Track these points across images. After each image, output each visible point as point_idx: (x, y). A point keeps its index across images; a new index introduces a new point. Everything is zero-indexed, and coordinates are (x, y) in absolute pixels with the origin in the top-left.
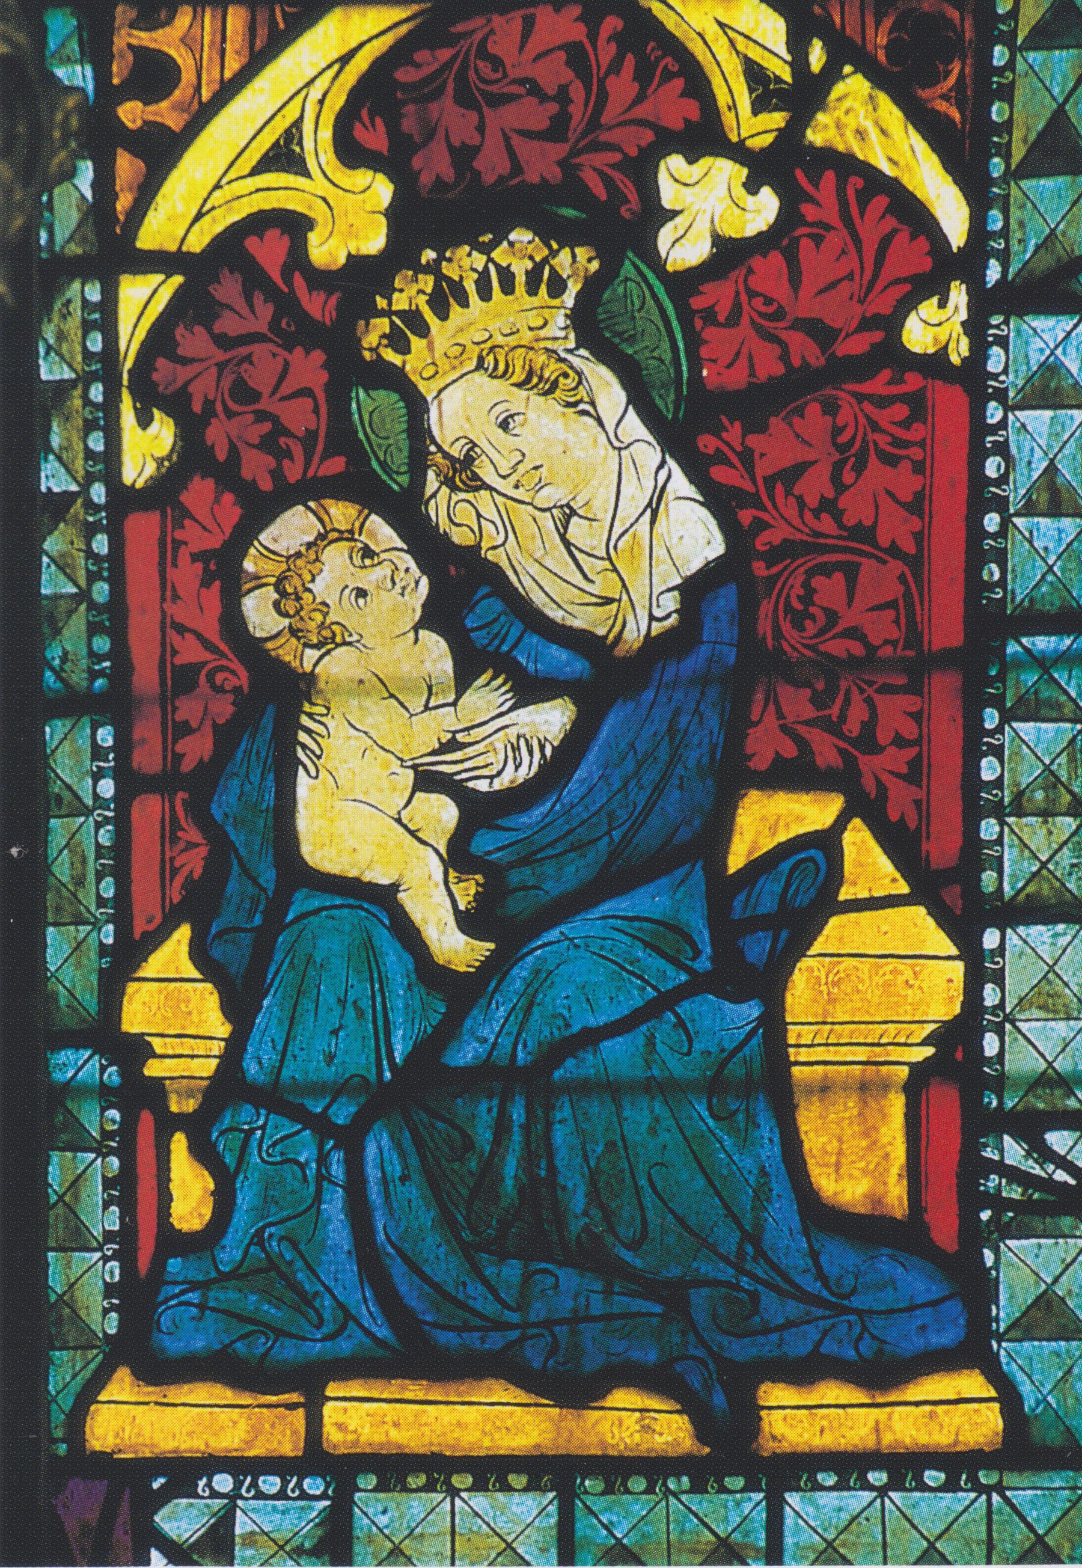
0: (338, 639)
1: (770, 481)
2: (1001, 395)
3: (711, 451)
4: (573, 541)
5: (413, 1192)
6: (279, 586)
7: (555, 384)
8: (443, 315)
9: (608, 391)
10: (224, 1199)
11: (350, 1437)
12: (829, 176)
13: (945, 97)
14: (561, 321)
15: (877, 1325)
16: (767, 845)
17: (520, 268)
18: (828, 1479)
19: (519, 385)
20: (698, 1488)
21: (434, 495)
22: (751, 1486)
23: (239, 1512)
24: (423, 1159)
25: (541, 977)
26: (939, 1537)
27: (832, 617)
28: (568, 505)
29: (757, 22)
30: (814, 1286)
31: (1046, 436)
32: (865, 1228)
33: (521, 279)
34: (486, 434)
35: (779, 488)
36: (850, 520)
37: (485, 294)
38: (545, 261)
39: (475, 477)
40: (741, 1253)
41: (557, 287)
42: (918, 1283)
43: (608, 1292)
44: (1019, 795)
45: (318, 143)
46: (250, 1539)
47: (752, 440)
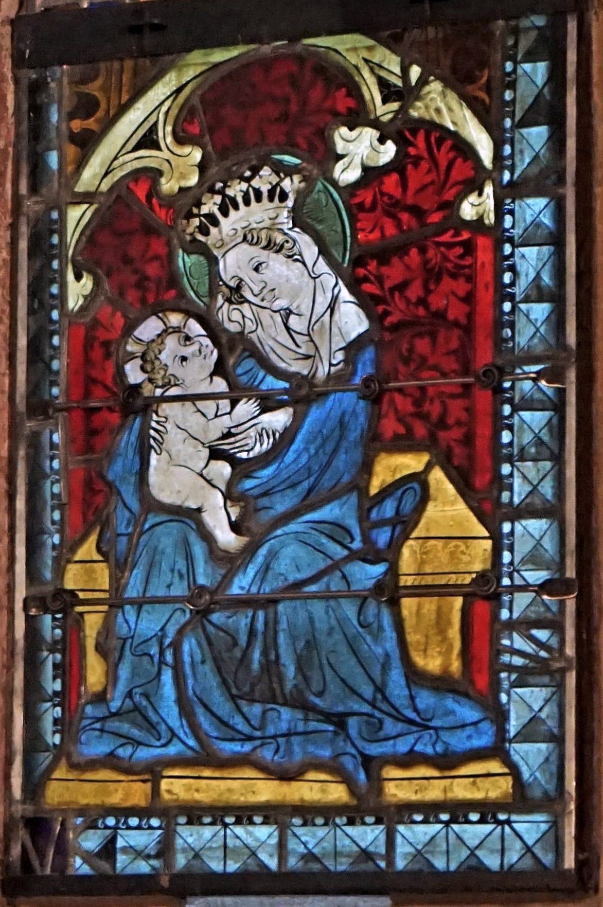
0: (172, 383)
1: (392, 290)
2: (511, 240)
3: (362, 275)
4: (291, 327)
5: (208, 669)
6: (143, 357)
7: (282, 247)
8: (225, 214)
9: (308, 248)
10: (112, 676)
11: (175, 797)
12: (421, 135)
13: (480, 89)
14: (285, 214)
15: (445, 736)
16: (389, 480)
17: (265, 189)
18: (418, 817)
19: (264, 248)
20: (351, 822)
21: (221, 307)
22: (378, 821)
23: (119, 837)
24: (212, 651)
25: (273, 555)
26: (477, 848)
27: (424, 359)
28: (288, 309)
29: (385, 57)
30: (412, 715)
31: (535, 260)
32: (441, 684)
33: (265, 194)
34: (248, 276)
35: (397, 294)
36: (433, 308)
37: (247, 203)
38: (278, 184)
39: (242, 296)
40: (375, 698)
41: (284, 197)
42: (468, 712)
43: (306, 720)
44: (522, 449)
45: (165, 135)
46: (124, 850)
47: (384, 270)
